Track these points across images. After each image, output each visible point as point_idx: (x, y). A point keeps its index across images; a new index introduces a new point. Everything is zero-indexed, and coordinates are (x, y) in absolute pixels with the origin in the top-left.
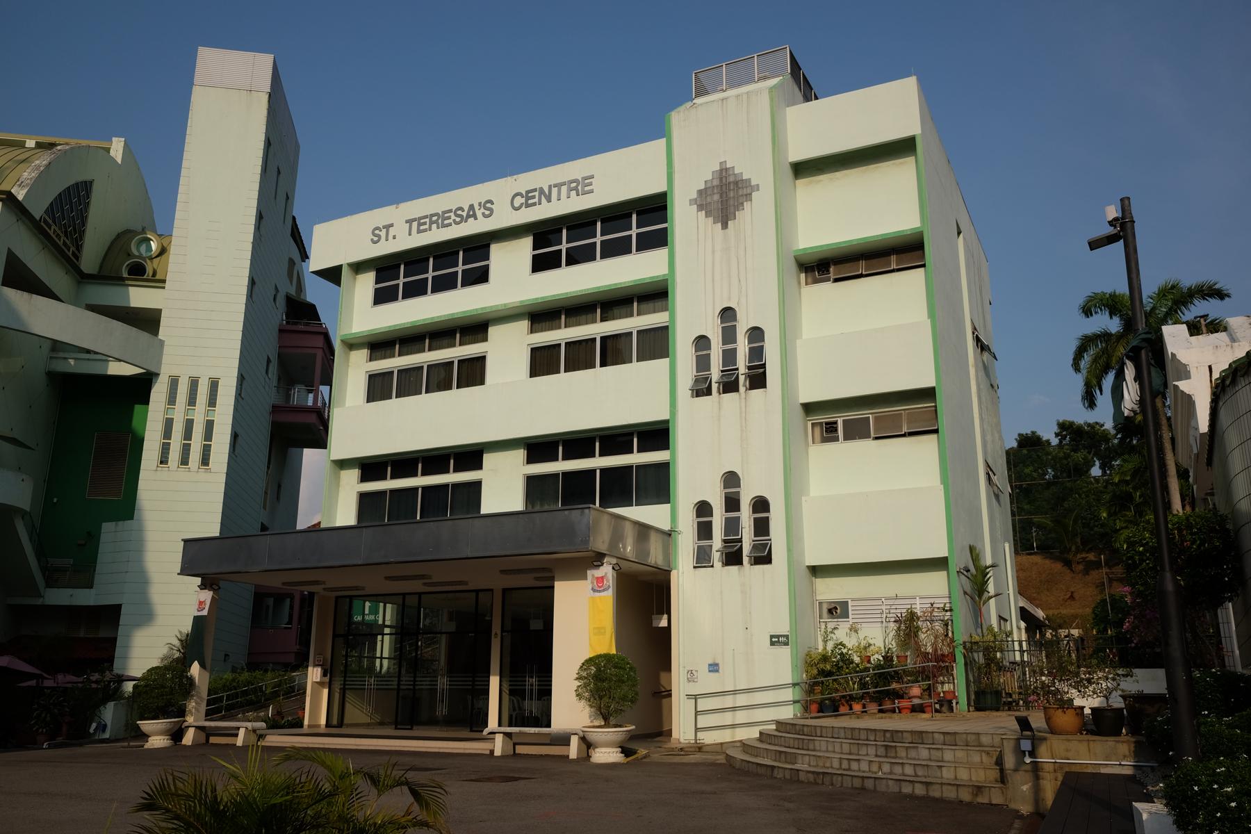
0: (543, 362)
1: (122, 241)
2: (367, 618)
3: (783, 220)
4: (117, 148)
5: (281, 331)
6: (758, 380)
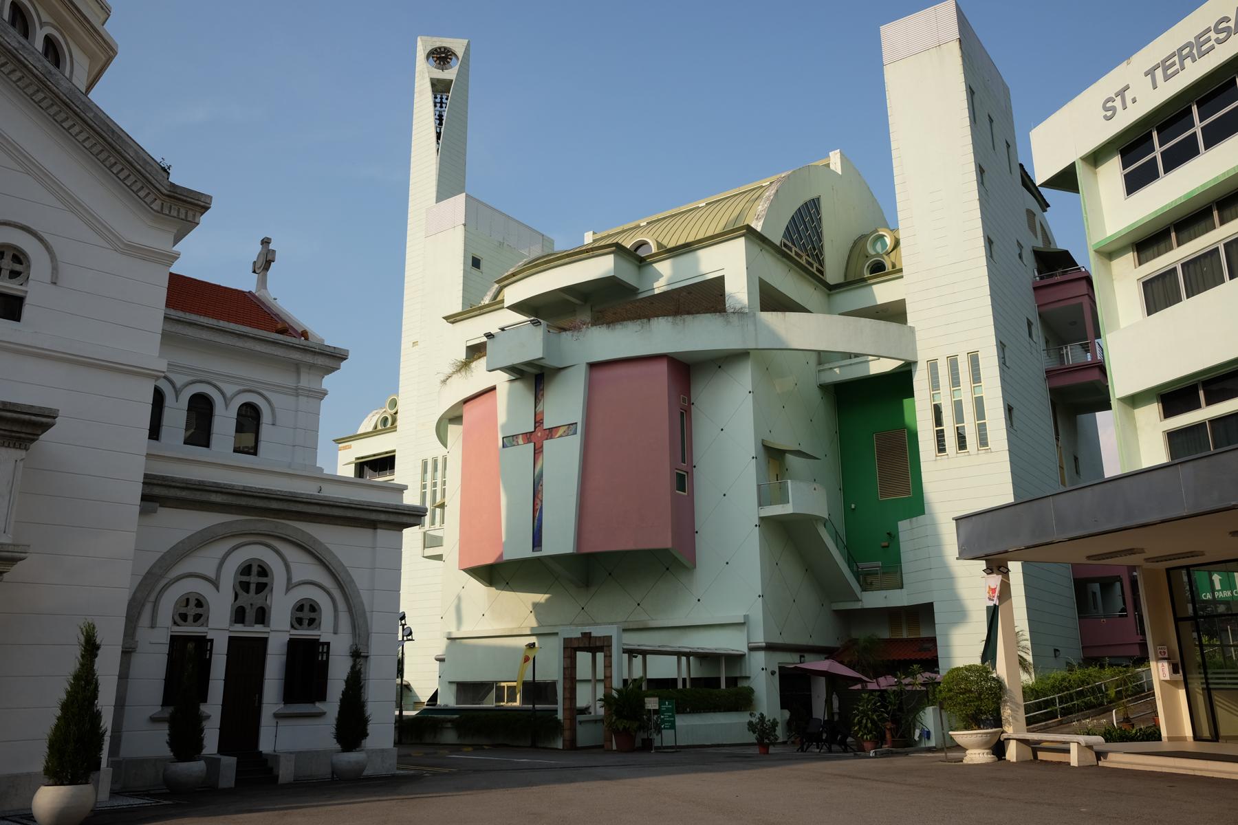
1: (858, 246)
2: (1219, 595)
4: (835, 160)
5: (1035, 289)
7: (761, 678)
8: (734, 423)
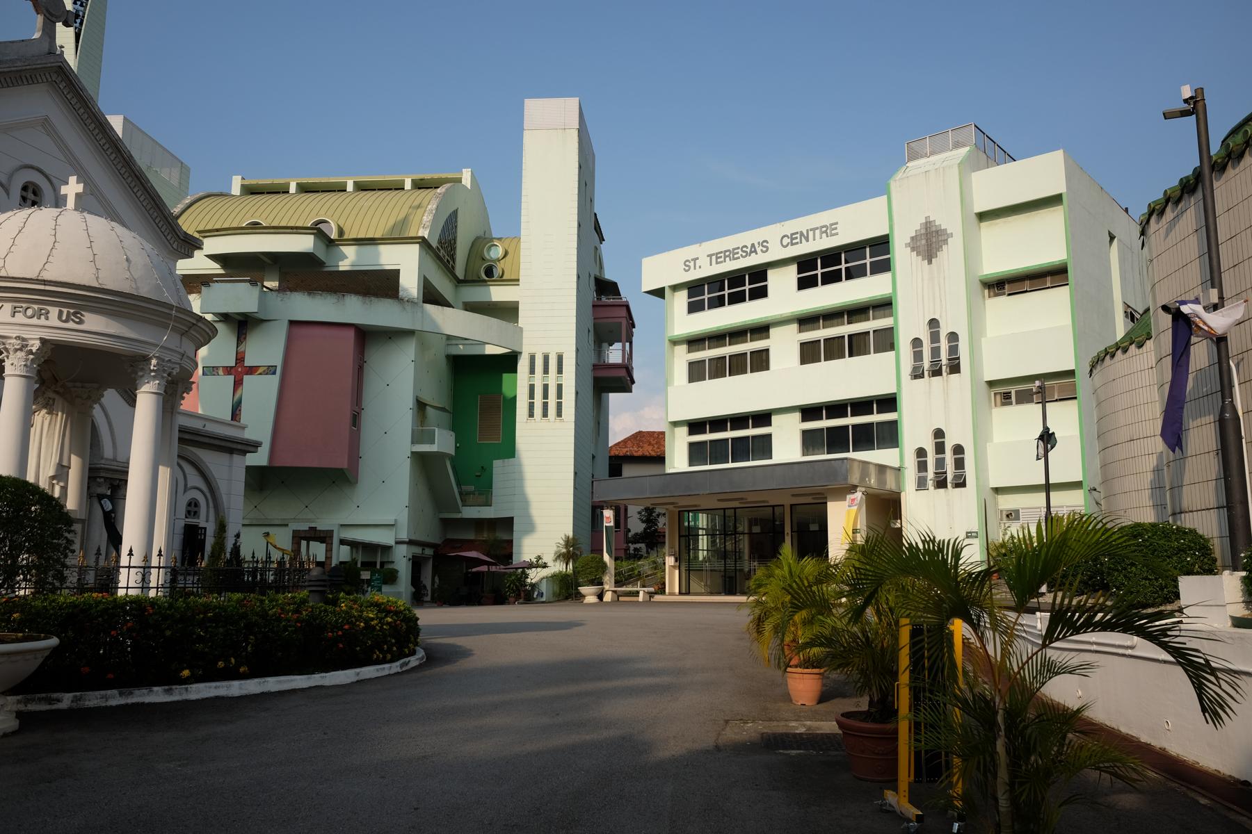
0: (809, 353)
3: (971, 254)
6: (955, 368)
7: (401, 560)
8: (399, 382)
